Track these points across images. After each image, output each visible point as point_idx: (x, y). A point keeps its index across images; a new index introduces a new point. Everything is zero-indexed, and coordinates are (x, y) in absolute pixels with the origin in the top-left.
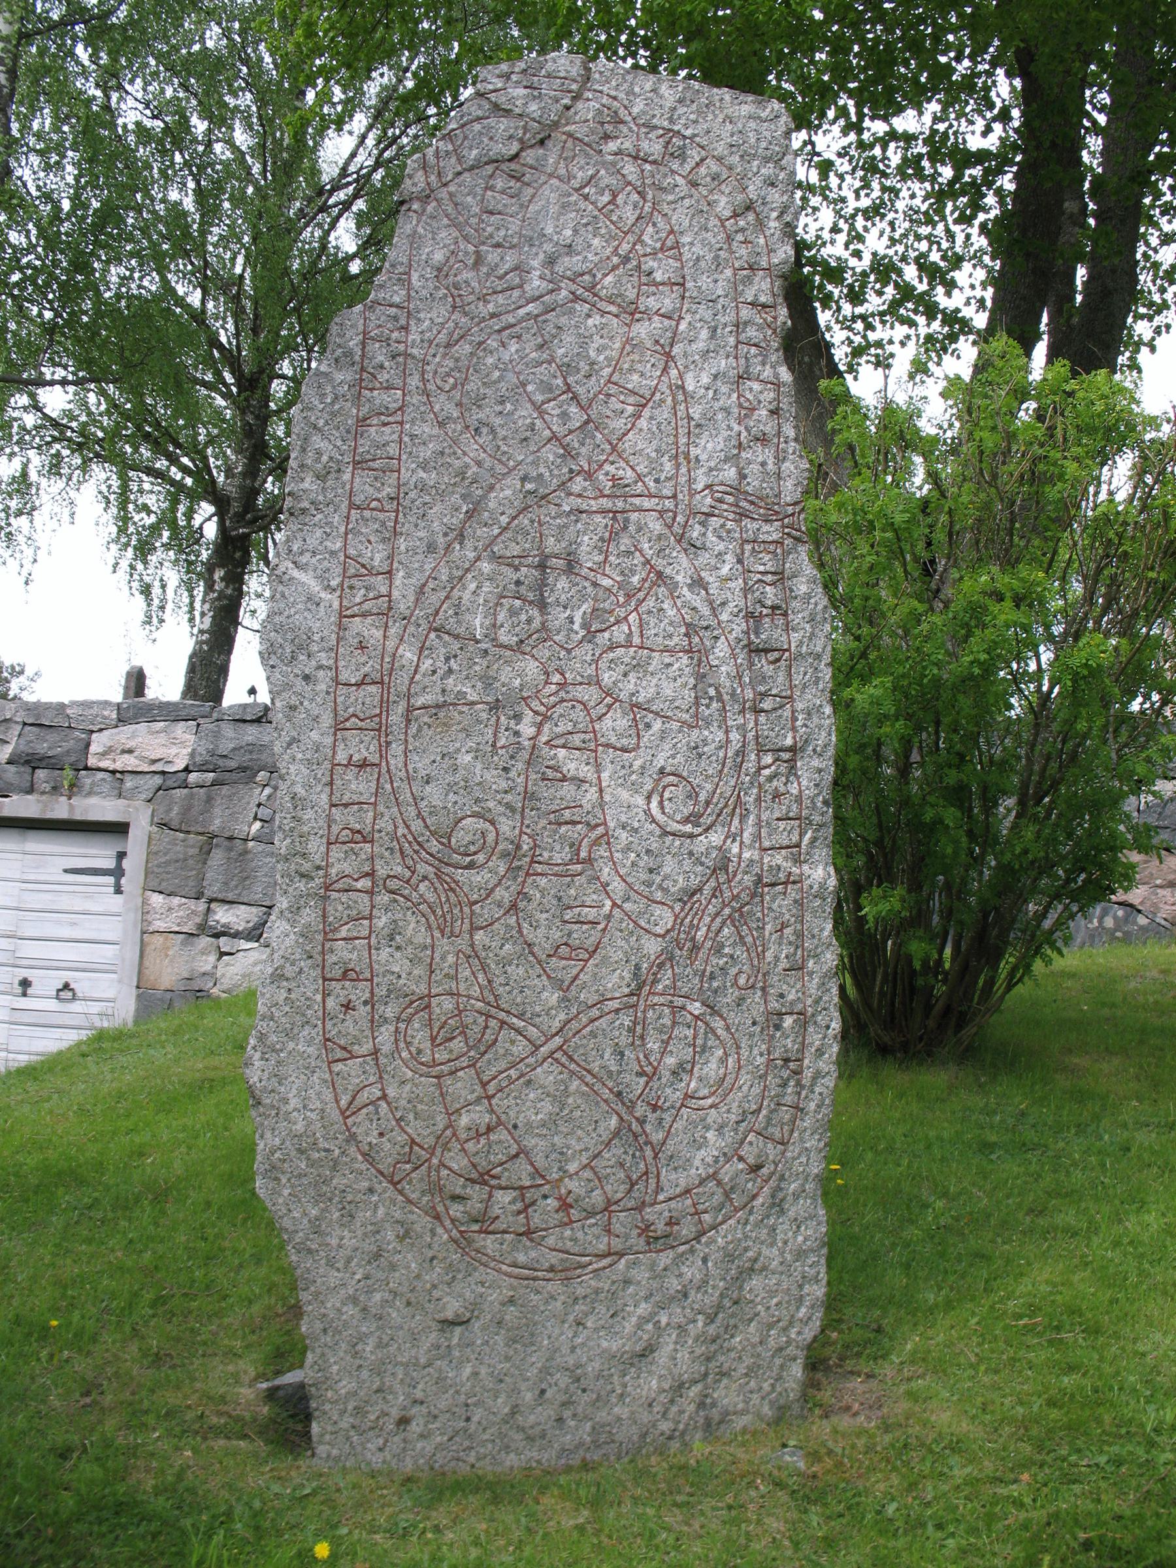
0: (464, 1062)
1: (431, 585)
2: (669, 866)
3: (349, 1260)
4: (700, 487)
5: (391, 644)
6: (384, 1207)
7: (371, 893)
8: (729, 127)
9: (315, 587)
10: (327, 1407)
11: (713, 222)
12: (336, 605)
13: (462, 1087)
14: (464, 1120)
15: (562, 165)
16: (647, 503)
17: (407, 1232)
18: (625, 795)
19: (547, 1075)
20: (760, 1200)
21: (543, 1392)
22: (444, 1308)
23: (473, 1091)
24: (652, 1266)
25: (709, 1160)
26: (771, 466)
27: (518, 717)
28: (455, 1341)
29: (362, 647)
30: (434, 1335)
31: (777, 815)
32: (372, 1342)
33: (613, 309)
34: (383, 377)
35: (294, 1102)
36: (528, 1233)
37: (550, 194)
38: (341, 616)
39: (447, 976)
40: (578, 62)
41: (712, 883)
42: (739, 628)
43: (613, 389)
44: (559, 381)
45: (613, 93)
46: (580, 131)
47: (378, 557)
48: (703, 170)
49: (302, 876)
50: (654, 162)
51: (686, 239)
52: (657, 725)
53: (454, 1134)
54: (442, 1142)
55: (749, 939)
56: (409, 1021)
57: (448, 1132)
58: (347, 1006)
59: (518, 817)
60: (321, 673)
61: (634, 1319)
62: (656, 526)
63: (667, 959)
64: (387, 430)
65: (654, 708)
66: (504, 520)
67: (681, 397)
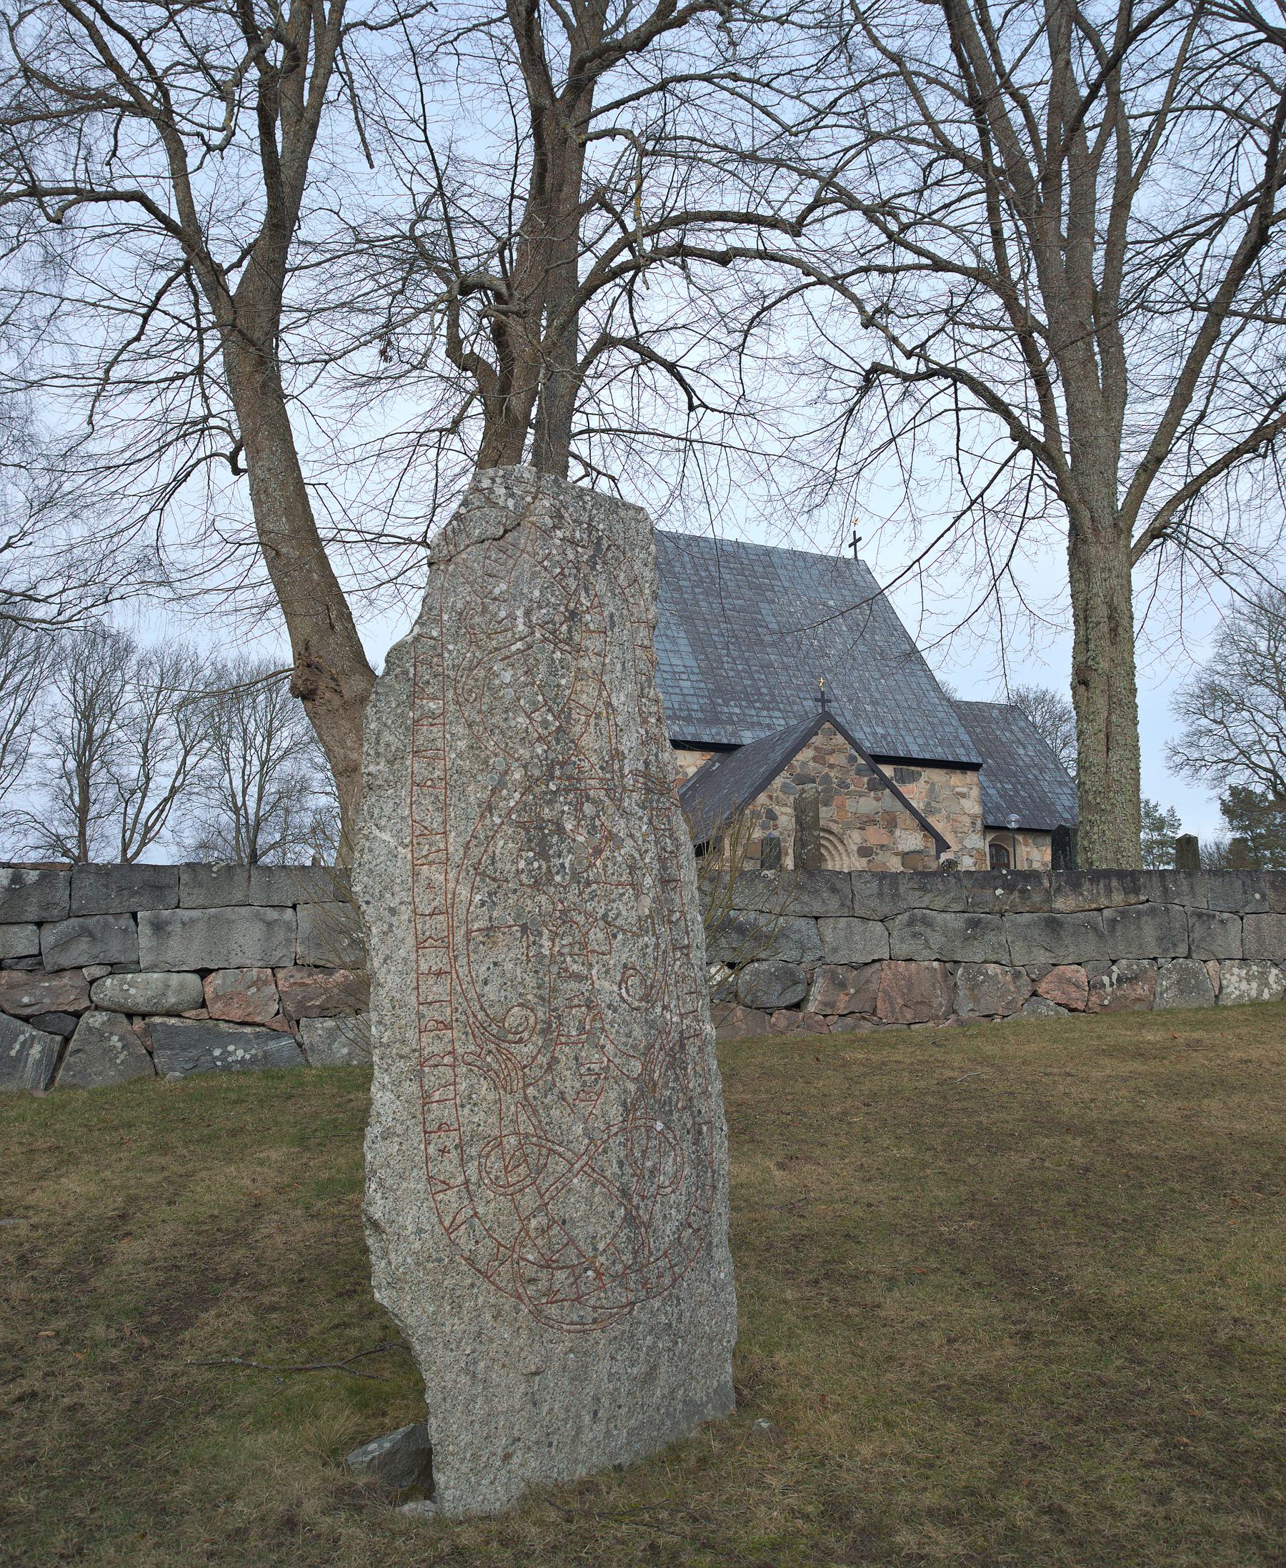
0: (529, 1180)
6: (485, 1295)
7: (453, 1066)
10: (450, 1458)
14: (534, 1223)
18: (607, 984)
29: (429, 886)
34: (430, 690)
49: (402, 1057)
56: (488, 1156)
58: (443, 1151)
64: (435, 729)
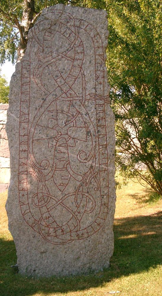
1: (36, 116)
2: (81, 168)
3: (24, 241)
4: (87, 94)
5: (29, 128)
8: (93, 17)
9: (15, 117)
11: (90, 38)
12: (19, 120)
13: (44, 209)
15: (59, 29)
16: (77, 98)
17: (35, 236)
19: (59, 208)
20: (100, 230)
21: (59, 265)
22: (41, 249)
23: (46, 210)
24: (79, 242)
25: (90, 222)
26: (102, 89)
27: (53, 141)
28: (43, 256)
30: (39, 255)
31: (103, 158)
32: (29, 256)
33: (70, 59)
35: (14, 213)
36: (56, 236)
37: (57, 36)
38: (20, 123)
39: (41, 189)
40: (62, 6)
41: (90, 171)
42: (95, 122)
43: (70, 76)
44: (60, 75)
45: (69, 12)
46: (63, 21)
47: (26, 111)
48: (88, 27)
50: (78, 27)
51: (84, 43)
52: (79, 142)
53: (42, 218)
54: (40, 220)
55: (97, 181)
57: (41, 218)
59: (53, 160)
60: (17, 134)
61: (76, 252)
62: (79, 103)
63: (81, 185)
65: (78, 138)
66: (49, 103)
67: (83, 76)
